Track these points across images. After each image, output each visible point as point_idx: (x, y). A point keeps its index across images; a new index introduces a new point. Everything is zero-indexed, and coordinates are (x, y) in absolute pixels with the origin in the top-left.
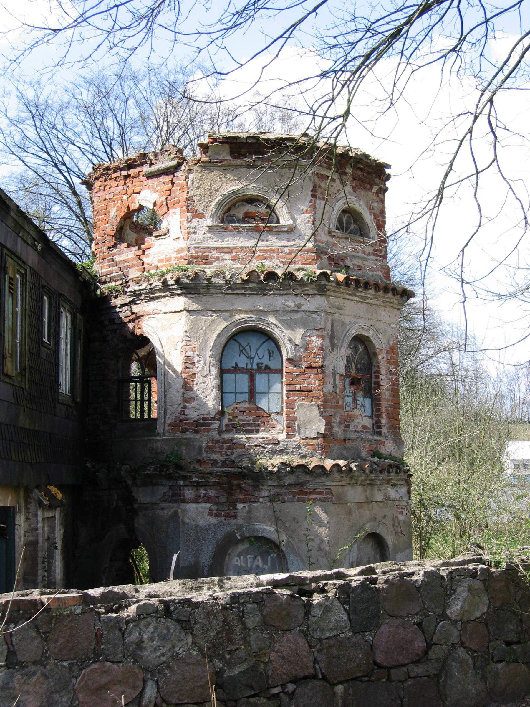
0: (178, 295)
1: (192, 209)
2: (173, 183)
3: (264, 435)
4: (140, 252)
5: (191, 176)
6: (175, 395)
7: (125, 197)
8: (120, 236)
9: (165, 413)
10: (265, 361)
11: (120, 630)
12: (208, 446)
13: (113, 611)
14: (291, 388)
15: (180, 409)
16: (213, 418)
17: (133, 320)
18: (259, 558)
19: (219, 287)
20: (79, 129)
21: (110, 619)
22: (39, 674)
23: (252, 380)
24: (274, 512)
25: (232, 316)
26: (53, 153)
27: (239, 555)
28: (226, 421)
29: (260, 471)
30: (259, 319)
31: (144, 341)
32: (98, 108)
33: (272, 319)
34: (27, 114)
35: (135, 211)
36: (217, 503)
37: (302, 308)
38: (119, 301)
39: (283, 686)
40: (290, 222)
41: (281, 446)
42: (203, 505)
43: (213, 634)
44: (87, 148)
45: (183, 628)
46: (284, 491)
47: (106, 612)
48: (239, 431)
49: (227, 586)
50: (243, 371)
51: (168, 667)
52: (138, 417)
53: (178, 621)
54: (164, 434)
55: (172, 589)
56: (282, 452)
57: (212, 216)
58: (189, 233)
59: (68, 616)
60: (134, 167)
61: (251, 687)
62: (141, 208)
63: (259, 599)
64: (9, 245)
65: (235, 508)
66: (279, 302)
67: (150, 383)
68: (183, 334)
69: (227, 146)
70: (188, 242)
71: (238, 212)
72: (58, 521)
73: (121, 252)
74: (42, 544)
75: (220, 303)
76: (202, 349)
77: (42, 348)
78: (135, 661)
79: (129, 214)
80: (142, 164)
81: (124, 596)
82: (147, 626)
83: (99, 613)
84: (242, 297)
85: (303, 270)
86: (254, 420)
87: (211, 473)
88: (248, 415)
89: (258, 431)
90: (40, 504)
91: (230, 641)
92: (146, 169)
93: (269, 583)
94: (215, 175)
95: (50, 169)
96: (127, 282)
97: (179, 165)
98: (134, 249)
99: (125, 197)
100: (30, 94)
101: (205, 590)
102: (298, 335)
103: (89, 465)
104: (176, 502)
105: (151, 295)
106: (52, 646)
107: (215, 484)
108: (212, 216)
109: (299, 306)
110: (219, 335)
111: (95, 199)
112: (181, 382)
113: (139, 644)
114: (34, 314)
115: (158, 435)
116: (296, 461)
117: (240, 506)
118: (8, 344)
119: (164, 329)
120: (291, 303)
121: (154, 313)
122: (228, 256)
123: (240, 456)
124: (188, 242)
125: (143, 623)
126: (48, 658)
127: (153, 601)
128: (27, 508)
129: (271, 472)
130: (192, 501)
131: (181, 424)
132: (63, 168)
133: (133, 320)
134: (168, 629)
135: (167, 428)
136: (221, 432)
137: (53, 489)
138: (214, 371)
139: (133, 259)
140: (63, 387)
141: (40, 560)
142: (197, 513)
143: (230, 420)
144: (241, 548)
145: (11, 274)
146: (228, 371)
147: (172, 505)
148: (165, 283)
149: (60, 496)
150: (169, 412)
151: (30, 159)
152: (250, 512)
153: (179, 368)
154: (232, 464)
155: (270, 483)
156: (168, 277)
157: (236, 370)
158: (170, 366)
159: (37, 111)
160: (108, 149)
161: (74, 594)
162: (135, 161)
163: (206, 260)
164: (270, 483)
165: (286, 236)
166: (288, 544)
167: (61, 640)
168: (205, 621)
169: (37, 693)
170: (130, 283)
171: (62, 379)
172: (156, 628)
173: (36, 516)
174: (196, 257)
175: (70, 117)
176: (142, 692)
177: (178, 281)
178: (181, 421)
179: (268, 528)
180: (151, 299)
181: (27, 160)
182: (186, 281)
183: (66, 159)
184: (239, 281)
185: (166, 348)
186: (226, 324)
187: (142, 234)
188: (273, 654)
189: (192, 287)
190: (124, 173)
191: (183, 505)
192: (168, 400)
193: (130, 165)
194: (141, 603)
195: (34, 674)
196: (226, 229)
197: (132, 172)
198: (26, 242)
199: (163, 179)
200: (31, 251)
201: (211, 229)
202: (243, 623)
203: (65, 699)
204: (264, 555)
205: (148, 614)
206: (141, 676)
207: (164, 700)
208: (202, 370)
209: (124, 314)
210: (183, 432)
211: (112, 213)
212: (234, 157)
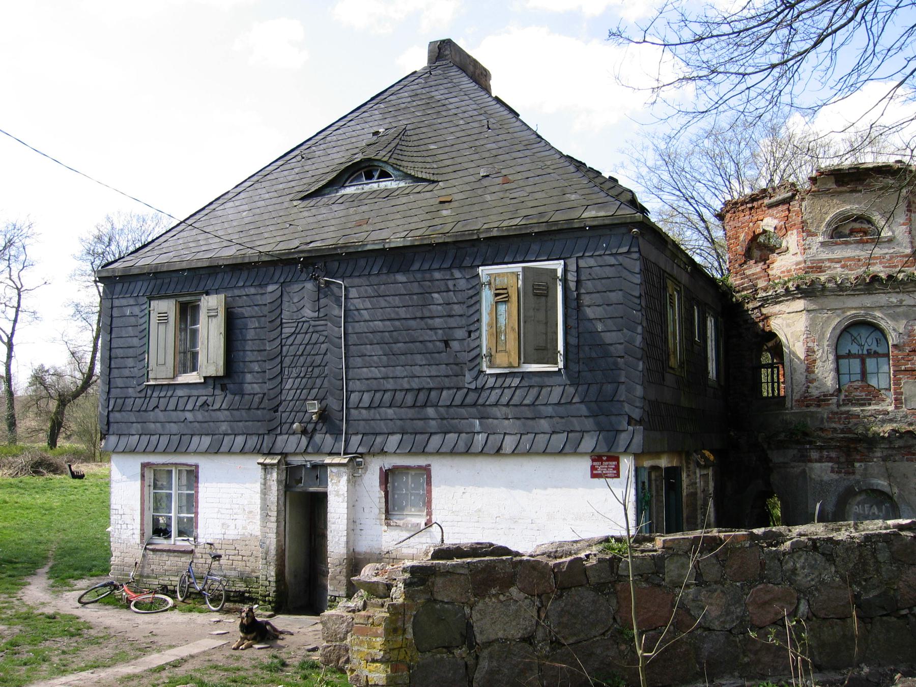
0: (799, 298)
1: (806, 230)
2: (789, 210)
3: (876, 407)
4: (766, 266)
5: (804, 204)
6: (800, 377)
7: (751, 224)
8: (748, 255)
9: (792, 391)
10: (874, 347)
11: (779, 560)
12: (828, 417)
13: (772, 546)
14: (897, 369)
15: (804, 389)
16: (832, 395)
17: (763, 320)
18: (874, 507)
19: (832, 290)
20: (704, 170)
21: (771, 552)
22: (719, 591)
23: (863, 363)
24: (887, 469)
25: (844, 312)
26: (684, 191)
27: (858, 504)
28: (842, 397)
29: (873, 437)
30: (867, 314)
31: (772, 335)
32: (717, 152)
33: (878, 314)
34: (661, 162)
35: (760, 234)
36: (838, 463)
37: (904, 303)
38: (750, 306)
39: (910, 609)
40: (890, 234)
41: (891, 416)
42: (826, 464)
43: (851, 565)
44: (710, 183)
45: (828, 560)
46: (895, 452)
47: (768, 547)
48: (854, 405)
49: (861, 528)
50: (855, 356)
51: (817, 589)
52: (770, 395)
53: (823, 554)
54: (792, 408)
55: (818, 530)
56: (891, 421)
57: (823, 233)
58: (805, 249)
59: (739, 548)
60: (758, 200)
61: (884, 608)
62: (765, 232)
63: (887, 539)
64: (668, 270)
65: (853, 466)
66: (882, 299)
67: (778, 368)
68: (803, 329)
69: (832, 177)
70: (805, 256)
71: (845, 230)
72: (710, 478)
73: (750, 268)
74: (700, 495)
75: (832, 302)
76: (821, 339)
77: (695, 346)
78: (791, 584)
79: (755, 237)
80: (763, 198)
81: (781, 534)
82: (799, 557)
83: (762, 547)
84: (852, 297)
85: (903, 272)
86: (866, 395)
87: (832, 439)
88: (861, 391)
89: (870, 404)
90: (698, 465)
91: (865, 571)
92: (767, 201)
93: (895, 526)
94: (824, 200)
95: (682, 203)
96: (756, 290)
97: (794, 196)
98: (761, 265)
99: (751, 224)
100: (662, 146)
101: (843, 531)
102: (901, 326)
103: (732, 433)
104: (804, 461)
105: (776, 300)
106: (728, 570)
107: (836, 447)
108: (823, 233)
109: (901, 301)
110: (834, 329)
111: (727, 228)
112: (804, 367)
113: (794, 571)
114: (687, 321)
115: (787, 409)
116: (905, 428)
117: (857, 465)
118: (671, 345)
119: (788, 325)
120: (894, 299)
121: (780, 313)
122: (838, 265)
123: (856, 424)
124: (805, 256)
125: (796, 555)
126: (726, 579)
127: (803, 538)
128: (688, 468)
129: (883, 437)
130: (816, 461)
131: (805, 399)
132: (692, 201)
133: (763, 320)
134: (816, 560)
135: (794, 403)
136: (838, 405)
137: (707, 453)
138: (831, 357)
139: (760, 272)
140: (711, 374)
141: (699, 508)
142: (821, 470)
143: (846, 396)
144: (859, 498)
145: (671, 292)
146: (843, 357)
147: (800, 464)
148: (787, 289)
149: (712, 458)
150: (795, 391)
151: (666, 197)
152: (866, 469)
153: (802, 357)
154: (850, 431)
155: (882, 446)
156: (790, 284)
157: (849, 355)
158: (794, 354)
159: (668, 159)
160: (727, 183)
161: (743, 532)
162: (757, 195)
163: (820, 270)
164: (882, 446)
165: (887, 245)
166: (900, 495)
167: (735, 567)
168: (845, 555)
169: (718, 605)
170: (759, 291)
171: (710, 368)
172: (806, 559)
173: (695, 473)
174: (812, 268)
175: (695, 161)
176: (797, 608)
177: (798, 287)
178: (805, 397)
179: (882, 482)
180: (776, 303)
181: (664, 197)
182: (804, 287)
183: (695, 194)
184: (849, 285)
185: (791, 341)
186: (839, 319)
187: (765, 251)
188: (901, 583)
189: (809, 290)
190: (749, 205)
191: (810, 465)
192: (794, 381)
193: (753, 199)
194: (794, 540)
195: (716, 590)
196: (836, 244)
197: (755, 204)
198: (679, 266)
199: (780, 208)
200: (684, 273)
201: (823, 244)
202: (875, 558)
203: (738, 610)
204: (879, 505)
205: (800, 549)
206: (796, 595)
207: (814, 615)
208: (821, 356)
209: (755, 315)
210: (807, 406)
211: (742, 237)
212: (839, 186)
